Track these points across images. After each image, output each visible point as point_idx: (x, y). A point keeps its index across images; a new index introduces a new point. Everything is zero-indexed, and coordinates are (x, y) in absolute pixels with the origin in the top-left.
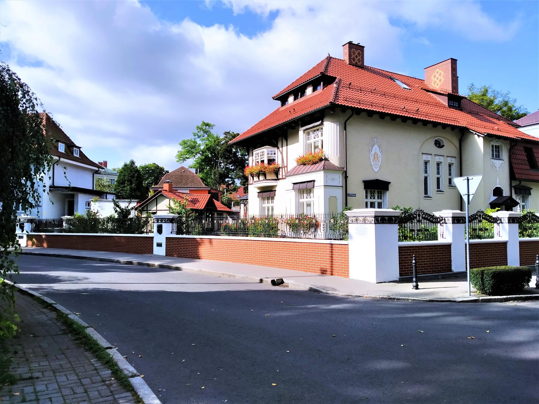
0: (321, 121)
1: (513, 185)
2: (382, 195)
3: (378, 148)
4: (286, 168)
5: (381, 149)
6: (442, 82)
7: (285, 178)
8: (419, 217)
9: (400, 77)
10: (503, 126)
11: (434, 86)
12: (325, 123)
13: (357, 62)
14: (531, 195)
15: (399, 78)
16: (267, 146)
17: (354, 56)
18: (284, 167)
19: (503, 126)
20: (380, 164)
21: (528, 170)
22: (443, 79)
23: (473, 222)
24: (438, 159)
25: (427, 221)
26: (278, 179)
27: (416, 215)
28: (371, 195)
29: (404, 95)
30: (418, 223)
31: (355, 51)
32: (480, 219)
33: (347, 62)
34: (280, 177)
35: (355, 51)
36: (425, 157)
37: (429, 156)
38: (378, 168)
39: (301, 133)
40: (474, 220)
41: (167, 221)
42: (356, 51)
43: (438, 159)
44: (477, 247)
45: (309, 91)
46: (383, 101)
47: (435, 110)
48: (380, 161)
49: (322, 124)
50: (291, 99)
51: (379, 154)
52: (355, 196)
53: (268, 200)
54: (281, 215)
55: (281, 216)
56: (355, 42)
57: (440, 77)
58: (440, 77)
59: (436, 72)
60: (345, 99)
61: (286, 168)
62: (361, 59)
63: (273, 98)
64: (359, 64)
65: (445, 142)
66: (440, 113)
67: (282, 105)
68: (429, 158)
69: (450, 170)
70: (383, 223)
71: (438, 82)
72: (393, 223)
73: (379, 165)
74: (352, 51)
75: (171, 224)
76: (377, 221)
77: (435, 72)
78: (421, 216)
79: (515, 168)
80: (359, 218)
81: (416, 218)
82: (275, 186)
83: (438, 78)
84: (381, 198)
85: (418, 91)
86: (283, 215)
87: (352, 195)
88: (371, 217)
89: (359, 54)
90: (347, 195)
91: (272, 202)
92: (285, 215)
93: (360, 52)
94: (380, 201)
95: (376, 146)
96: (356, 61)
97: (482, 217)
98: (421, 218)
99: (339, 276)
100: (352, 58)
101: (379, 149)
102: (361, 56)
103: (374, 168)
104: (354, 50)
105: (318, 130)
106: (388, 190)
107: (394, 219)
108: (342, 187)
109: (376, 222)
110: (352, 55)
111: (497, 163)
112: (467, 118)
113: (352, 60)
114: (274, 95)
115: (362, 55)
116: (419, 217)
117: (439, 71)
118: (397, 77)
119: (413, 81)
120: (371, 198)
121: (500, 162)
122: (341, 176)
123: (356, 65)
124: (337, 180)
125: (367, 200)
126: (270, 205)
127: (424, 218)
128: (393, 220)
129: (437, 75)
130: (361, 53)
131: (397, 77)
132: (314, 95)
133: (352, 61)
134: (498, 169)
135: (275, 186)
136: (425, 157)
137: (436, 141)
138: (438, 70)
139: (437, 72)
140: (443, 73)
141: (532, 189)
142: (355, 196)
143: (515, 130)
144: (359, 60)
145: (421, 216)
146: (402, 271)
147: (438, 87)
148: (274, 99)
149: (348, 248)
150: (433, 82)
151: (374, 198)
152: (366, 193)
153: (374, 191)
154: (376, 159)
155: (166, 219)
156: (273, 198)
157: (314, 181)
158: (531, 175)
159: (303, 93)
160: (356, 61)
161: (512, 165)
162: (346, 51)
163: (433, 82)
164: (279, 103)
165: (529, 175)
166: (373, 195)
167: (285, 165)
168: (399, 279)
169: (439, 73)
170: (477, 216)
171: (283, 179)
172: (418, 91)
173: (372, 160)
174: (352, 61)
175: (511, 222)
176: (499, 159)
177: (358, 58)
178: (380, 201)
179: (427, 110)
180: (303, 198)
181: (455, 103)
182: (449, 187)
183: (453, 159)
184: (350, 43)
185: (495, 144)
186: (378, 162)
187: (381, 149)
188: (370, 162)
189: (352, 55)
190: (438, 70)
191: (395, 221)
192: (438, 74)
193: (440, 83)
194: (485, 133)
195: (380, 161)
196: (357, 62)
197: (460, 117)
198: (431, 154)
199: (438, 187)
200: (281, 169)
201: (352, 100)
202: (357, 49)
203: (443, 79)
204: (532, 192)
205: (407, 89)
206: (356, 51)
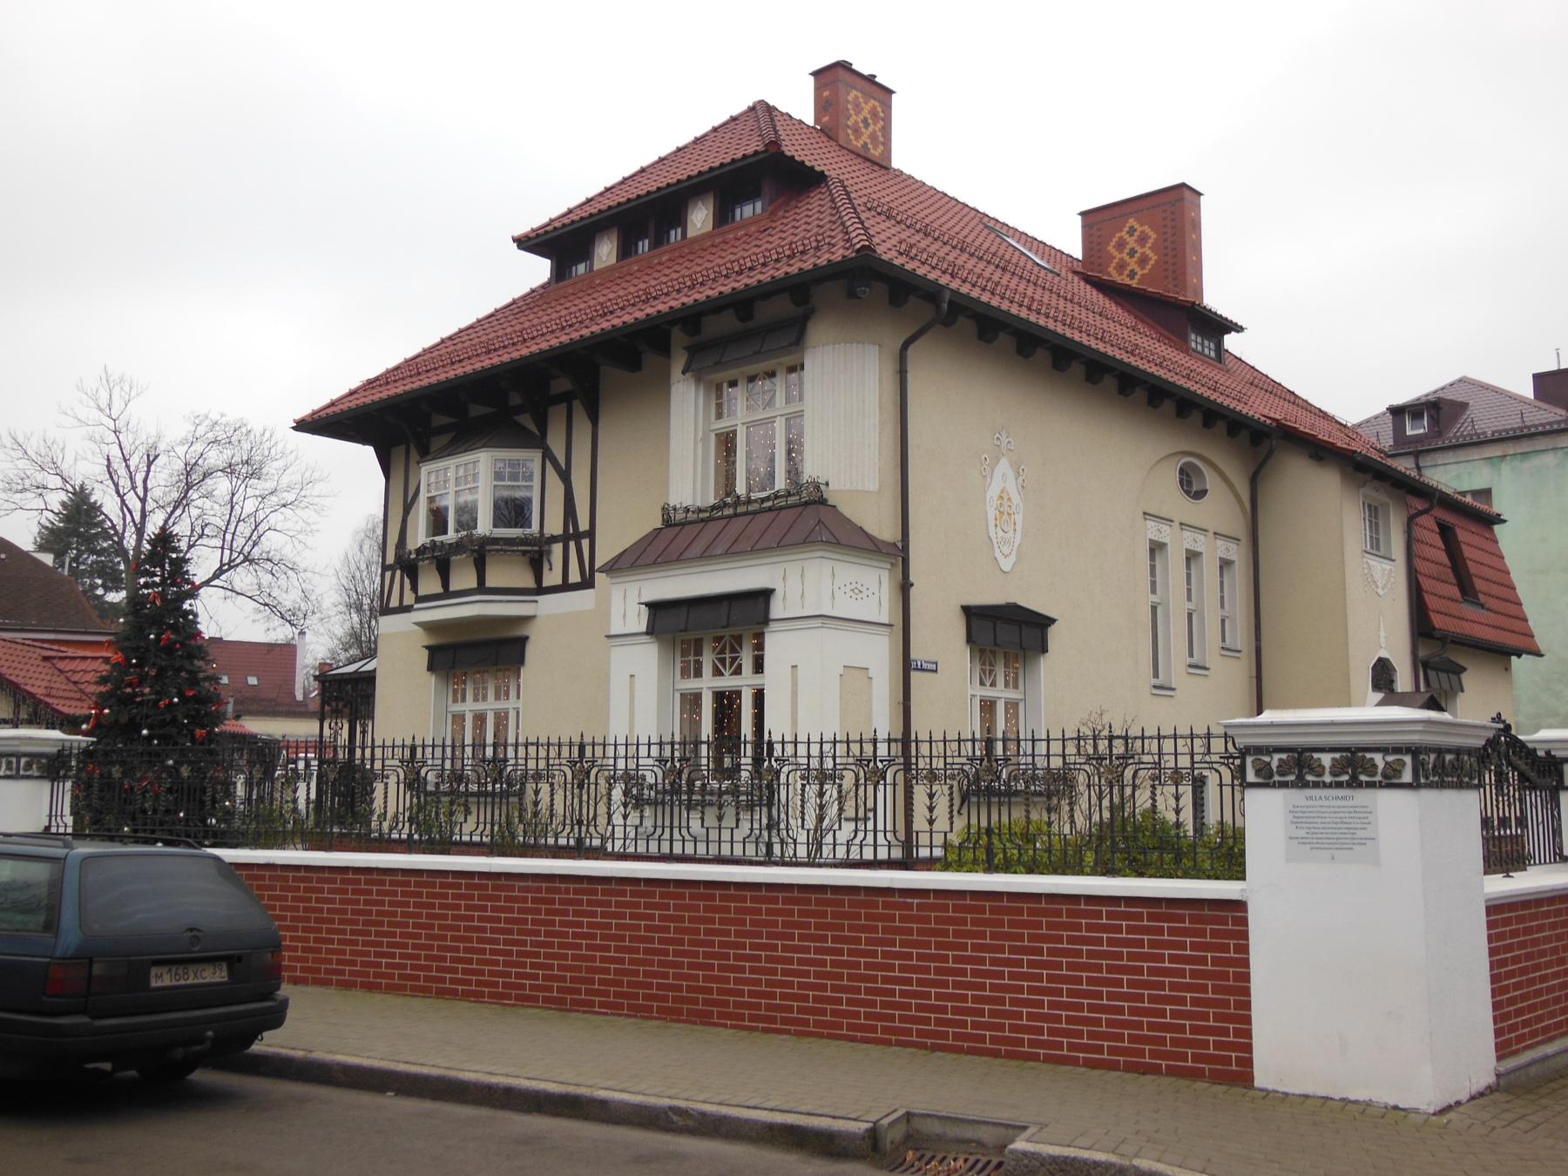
1: (1422, 653)
3: (1011, 475)
4: (585, 543)
5: (1020, 480)
6: (1149, 267)
13: (866, 143)
18: (578, 536)
20: (997, 550)
21: (1457, 601)
24: (1190, 540)
26: (541, 590)
28: (984, 672)
31: (861, 100)
34: (552, 577)
35: (861, 100)
36: (1154, 531)
38: (1013, 558)
41: (29, 766)
42: (866, 103)
48: (1019, 528)
50: (605, 252)
51: (1016, 499)
52: (936, 671)
55: (576, 750)
57: (1143, 246)
59: (1126, 229)
61: (585, 543)
62: (879, 134)
64: (875, 153)
65: (1211, 481)
68: (1165, 534)
71: (1132, 264)
73: (1016, 545)
74: (850, 98)
75: (45, 787)
77: (1121, 231)
79: (1427, 592)
83: (1132, 253)
84: (1016, 687)
87: (925, 666)
89: (874, 113)
90: (908, 666)
92: (449, 742)
93: (879, 109)
94: (1013, 695)
95: (1004, 466)
99: (1094, 1067)
101: (1016, 479)
102: (882, 123)
103: (998, 555)
104: (857, 97)
105: (772, 375)
106: (1044, 650)
108: (887, 630)
110: (852, 112)
111: (1379, 567)
113: (849, 131)
114: (523, 228)
115: (883, 120)
117: (1136, 226)
121: (1385, 566)
122: (885, 576)
123: (862, 153)
124: (870, 593)
126: (490, 705)
128: (1318, 770)
129: (1132, 242)
130: (882, 115)
133: (852, 137)
134: (1380, 592)
136: (1154, 531)
138: (1132, 222)
139: (1132, 231)
140: (1153, 235)
142: (936, 671)
144: (873, 137)
150: (1113, 265)
151: (993, 684)
154: (1006, 515)
155: (18, 756)
157: (765, 595)
158: (1467, 620)
160: (865, 138)
161: (1418, 583)
163: (1113, 265)
164: (539, 270)
165: (1463, 619)
167: (584, 525)
168: (1498, 1076)
169: (1137, 234)
171: (566, 587)
173: (992, 523)
174: (852, 137)
176: (1378, 553)
177: (871, 129)
178: (1013, 695)
181: (1206, 343)
182: (1224, 653)
183: (1233, 546)
186: (1011, 534)
187: (1020, 480)
188: (987, 526)
189: (852, 112)
190: (1132, 222)
192: (1135, 238)
193: (1143, 268)
195: (1019, 528)
198: (1172, 521)
199: (518, 713)
200: (557, 549)
202: (868, 96)
206: (866, 103)
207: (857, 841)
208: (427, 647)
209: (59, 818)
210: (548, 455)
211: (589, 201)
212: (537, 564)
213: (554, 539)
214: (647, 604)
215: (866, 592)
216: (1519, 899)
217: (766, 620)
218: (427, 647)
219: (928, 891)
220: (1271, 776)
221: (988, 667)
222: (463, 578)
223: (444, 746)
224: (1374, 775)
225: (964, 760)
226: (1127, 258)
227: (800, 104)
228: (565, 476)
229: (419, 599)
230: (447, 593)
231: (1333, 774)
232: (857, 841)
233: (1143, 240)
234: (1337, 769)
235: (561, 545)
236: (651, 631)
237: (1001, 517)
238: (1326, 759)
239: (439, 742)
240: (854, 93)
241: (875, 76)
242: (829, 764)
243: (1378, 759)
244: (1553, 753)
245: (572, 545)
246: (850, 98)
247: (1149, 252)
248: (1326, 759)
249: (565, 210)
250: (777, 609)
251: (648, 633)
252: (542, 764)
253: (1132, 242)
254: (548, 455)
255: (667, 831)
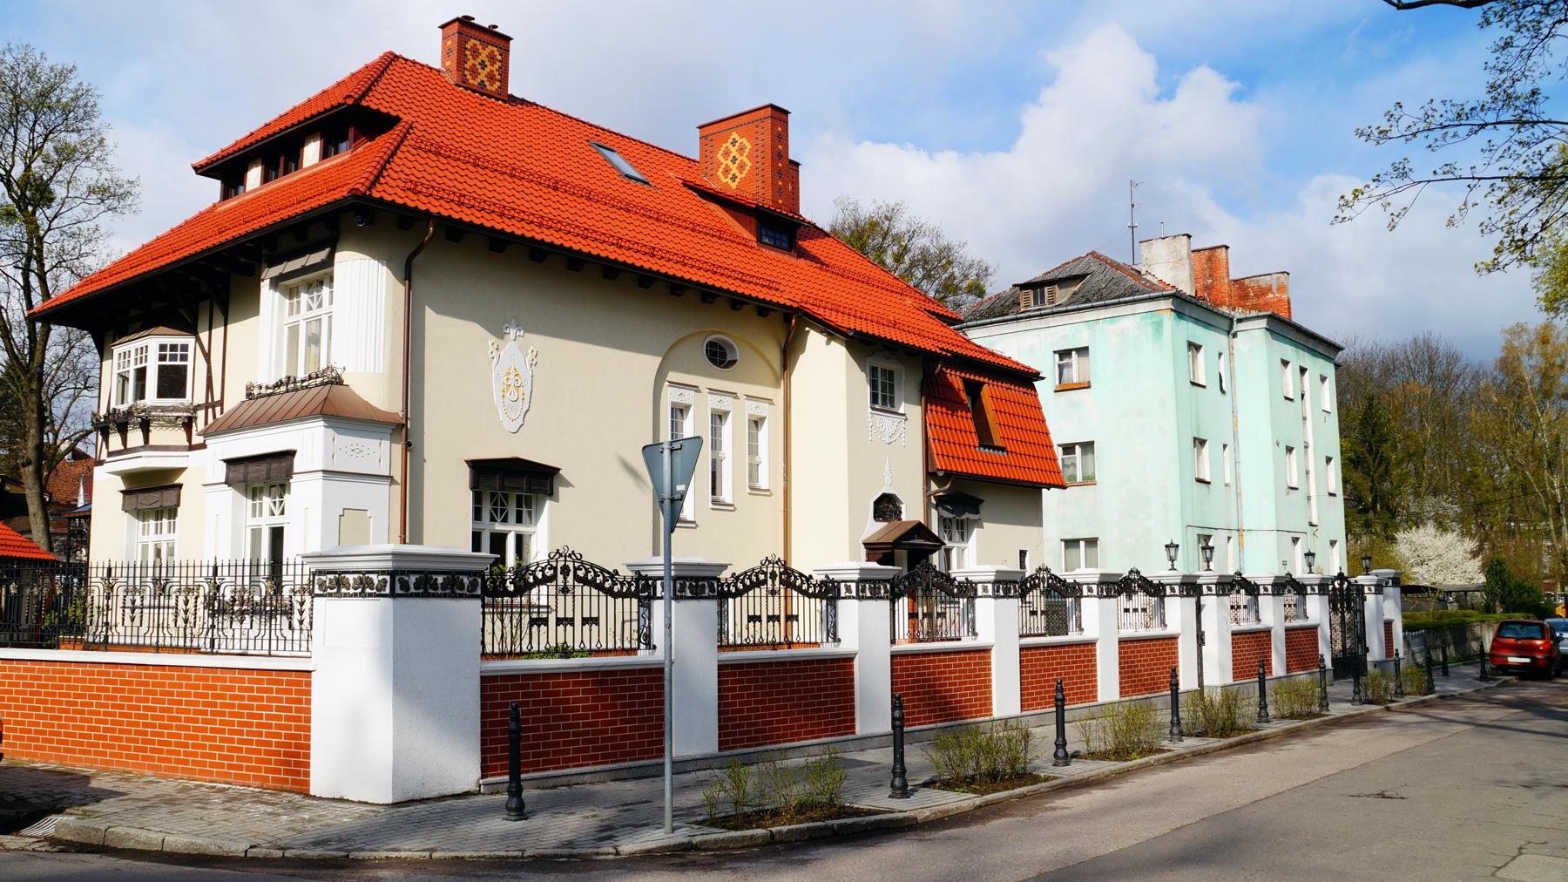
0: (328, 250)
2: (533, 510)
7: (203, 446)
8: (773, 582)
9: (660, 155)
10: (912, 316)
11: (724, 181)
12: (339, 256)
14: (559, 470)
15: (618, 145)
16: (161, 329)
17: (476, 63)
18: (214, 406)
19: (912, 316)
22: (750, 164)
23: (751, 593)
25: (595, 592)
27: (555, 569)
29: (623, 196)
30: (770, 599)
32: (773, 585)
33: (451, 78)
37: (728, 400)
39: (267, 294)
40: (754, 585)
42: (484, 49)
43: (752, 409)
44: (619, 682)
45: (311, 152)
46: (502, 190)
47: (712, 251)
49: (329, 262)
50: (254, 176)
53: (157, 520)
54: (106, 566)
55: (211, 570)
56: (482, 21)
58: (742, 155)
60: (409, 185)
63: (195, 168)
66: (728, 261)
67: (226, 195)
69: (753, 438)
70: (426, 595)
72: (462, 596)
74: (468, 46)
76: (401, 589)
77: (726, 142)
78: (571, 573)
80: (347, 576)
81: (765, 582)
82: (179, 471)
85: (672, 191)
86: (219, 564)
88: (383, 573)
89: (492, 57)
91: (172, 529)
92: (138, 565)
96: (482, 76)
97: (780, 577)
98: (570, 578)
100: (467, 66)
107: (688, 591)
109: (398, 591)
110: (469, 57)
112: (809, 284)
116: (565, 578)
117: (737, 138)
118: (605, 141)
119: (662, 160)
120: (493, 519)
125: (479, 526)
127: (584, 581)
128: (435, 586)
129: (734, 151)
130: (499, 58)
131: (605, 141)
132: (327, 165)
133: (469, 77)
135: (179, 471)
137: (711, 344)
138: (734, 135)
139: (734, 142)
141: (983, 501)
143: (945, 330)
144: (491, 77)
145: (571, 573)
146: (726, 735)
147: (734, 185)
148: (200, 174)
149: (309, 684)
151: (505, 520)
152: (477, 499)
153: (506, 496)
156: (172, 513)
157: (290, 454)
159: (295, 158)
160: (482, 76)
162: (449, 43)
164: (214, 187)
166: (502, 511)
167: (217, 397)
169: (737, 144)
170: (762, 577)
172: (672, 191)
175: (869, 594)
177: (487, 70)
179: (686, 249)
180: (261, 515)
184: (465, 22)
185: (882, 364)
189: (469, 57)
190: (734, 135)
191: (473, 586)
194: (850, 329)
196: (482, 81)
197: (787, 277)
201: (435, 192)
203: (750, 164)
204: (982, 508)
205: (637, 180)
206: (484, 49)
207: (260, 637)
208: (122, 492)
209: (165, 629)
210: (198, 340)
211: (252, 134)
212: (188, 425)
213: (199, 407)
214: (225, 461)
215: (366, 452)
216: (541, 672)
217: (289, 473)
218: (122, 492)
219: (538, 675)
220: (436, 589)
221: (499, 507)
222: (135, 438)
223: (135, 567)
224: (463, 589)
225: (202, 579)
226: (730, 164)
227: (429, 50)
228: (207, 356)
229: (110, 454)
230: (126, 450)
231: (443, 589)
232: (260, 637)
233: (741, 150)
234: (444, 586)
235: (203, 411)
236: (228, 482)
237: (508, 389)
238: (351, 578)
239: (233, 563)
240: (473, 41)
241: (496, 27)
242: (190, 582)
243: (374, 577)
244: (643, 574)
245: (210, 410)
246: (468, 46)
247: (746, 160)
248: (440, 579)
249: (248, 133)
250: (298, 464)
251: (226, 483)
252: (138, 583)
253: (734, 151)
254: (198, 340)
255: (268, 632)
